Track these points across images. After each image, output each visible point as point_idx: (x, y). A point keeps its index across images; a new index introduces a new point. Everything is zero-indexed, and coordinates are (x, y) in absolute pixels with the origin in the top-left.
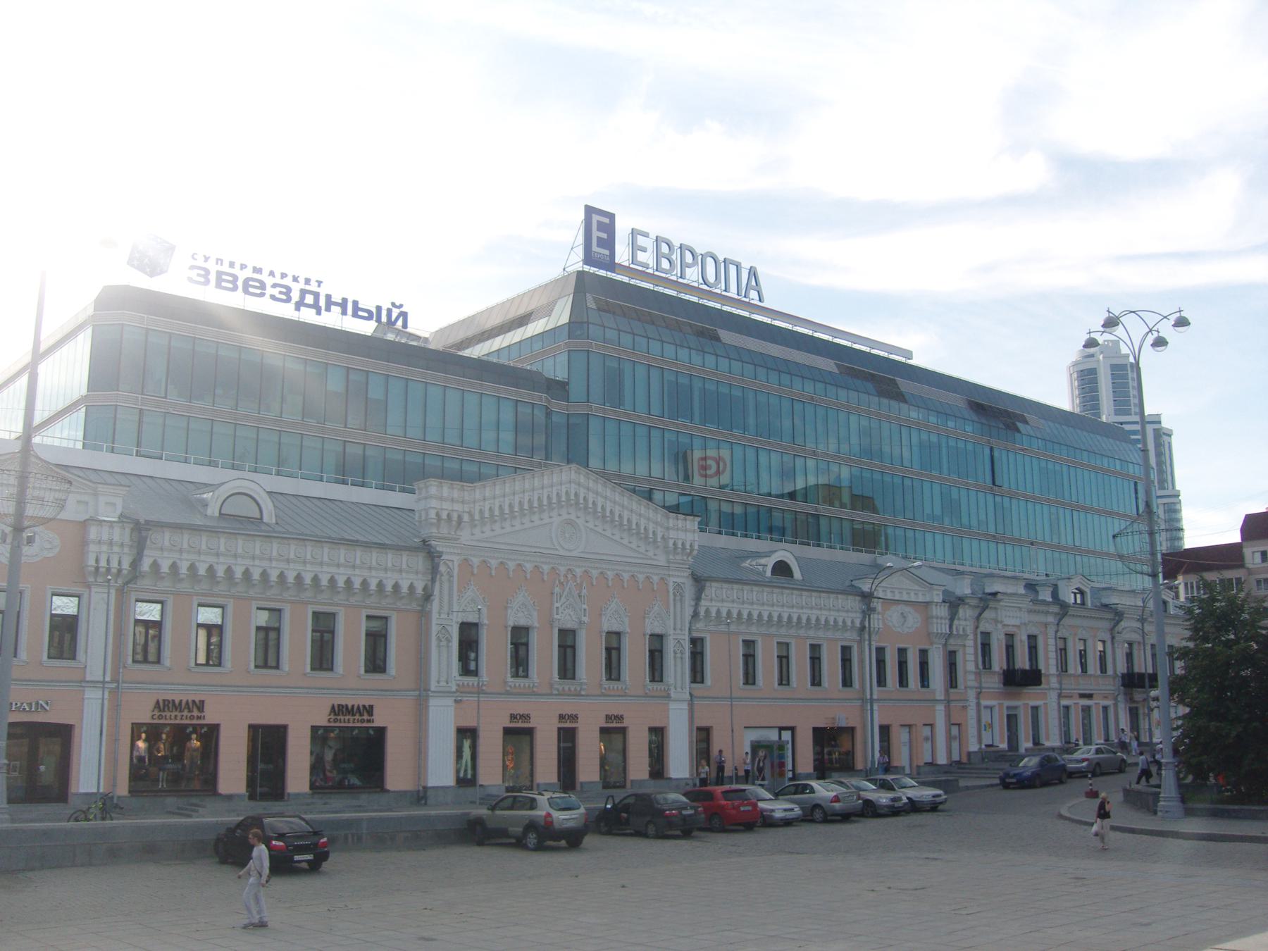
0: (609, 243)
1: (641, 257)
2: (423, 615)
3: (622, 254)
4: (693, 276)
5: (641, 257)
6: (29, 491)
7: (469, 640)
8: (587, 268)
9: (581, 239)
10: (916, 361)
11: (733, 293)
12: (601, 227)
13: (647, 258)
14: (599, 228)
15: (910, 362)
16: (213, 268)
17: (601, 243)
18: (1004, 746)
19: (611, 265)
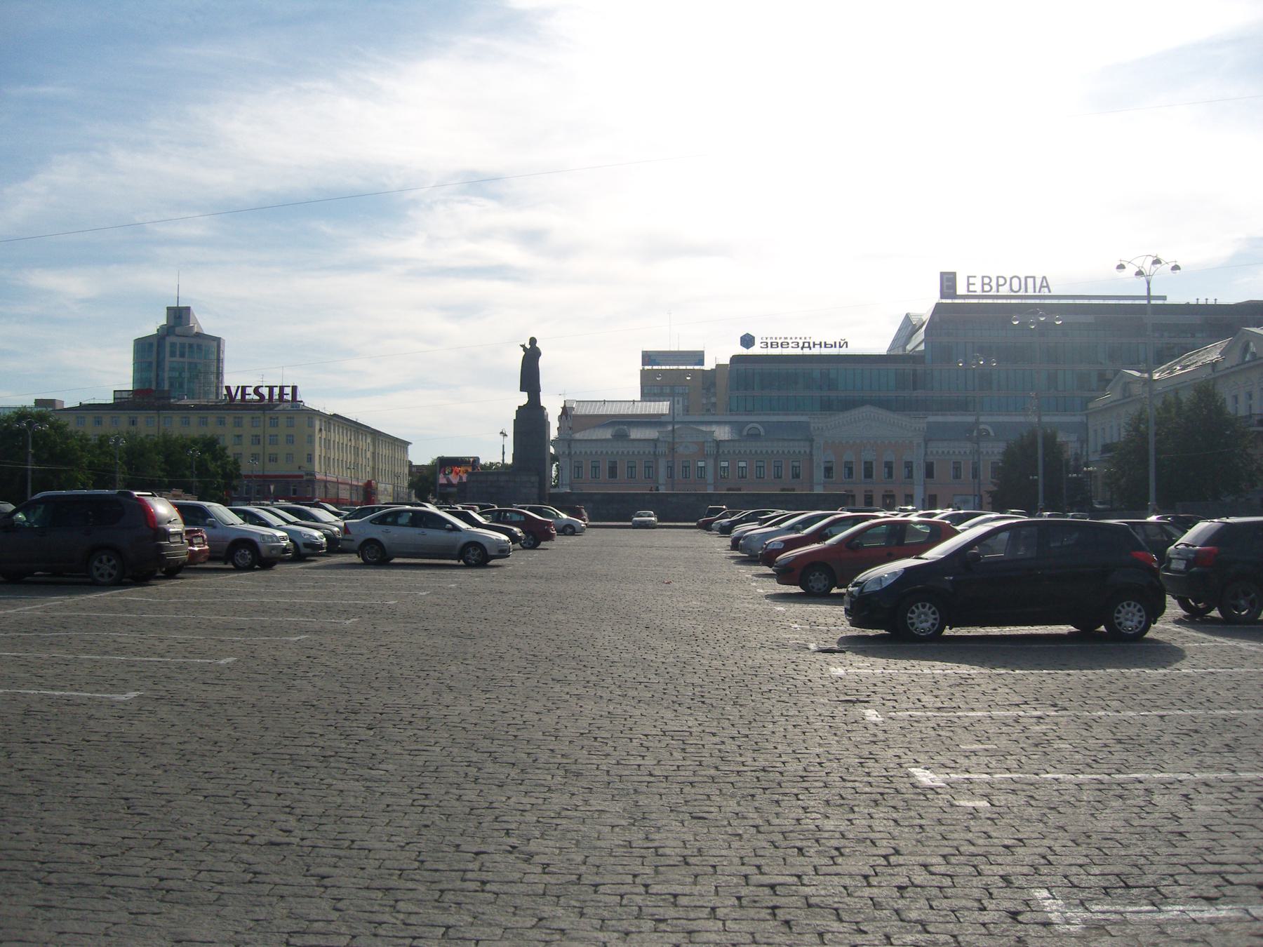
0: (954, 287)
1: (972, 288)
2: (811, 460)
3: (961, 289)
4: (1004, 290)
5: (972, 288)
6: (818, 490)
7: (828, 471)
8: (944, 301)
9: (1032, 677)
10: (1169, 301)
11: (1030, 292)
12: (948, 280)
13: (977, 289)
14: (948, 282)
15: (1167, 302)
16: (769, 341)
17: (948, 287)
18: (42, 507)
19: (955, 296)
